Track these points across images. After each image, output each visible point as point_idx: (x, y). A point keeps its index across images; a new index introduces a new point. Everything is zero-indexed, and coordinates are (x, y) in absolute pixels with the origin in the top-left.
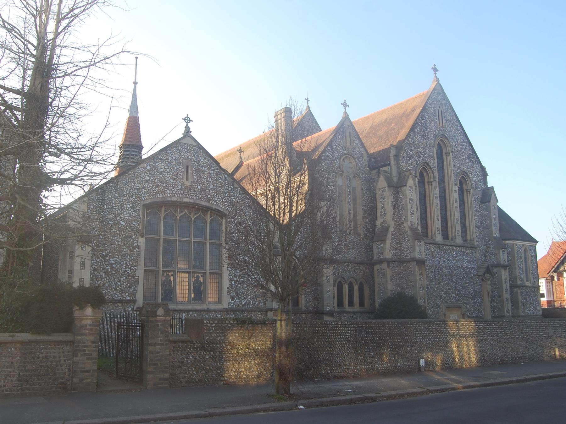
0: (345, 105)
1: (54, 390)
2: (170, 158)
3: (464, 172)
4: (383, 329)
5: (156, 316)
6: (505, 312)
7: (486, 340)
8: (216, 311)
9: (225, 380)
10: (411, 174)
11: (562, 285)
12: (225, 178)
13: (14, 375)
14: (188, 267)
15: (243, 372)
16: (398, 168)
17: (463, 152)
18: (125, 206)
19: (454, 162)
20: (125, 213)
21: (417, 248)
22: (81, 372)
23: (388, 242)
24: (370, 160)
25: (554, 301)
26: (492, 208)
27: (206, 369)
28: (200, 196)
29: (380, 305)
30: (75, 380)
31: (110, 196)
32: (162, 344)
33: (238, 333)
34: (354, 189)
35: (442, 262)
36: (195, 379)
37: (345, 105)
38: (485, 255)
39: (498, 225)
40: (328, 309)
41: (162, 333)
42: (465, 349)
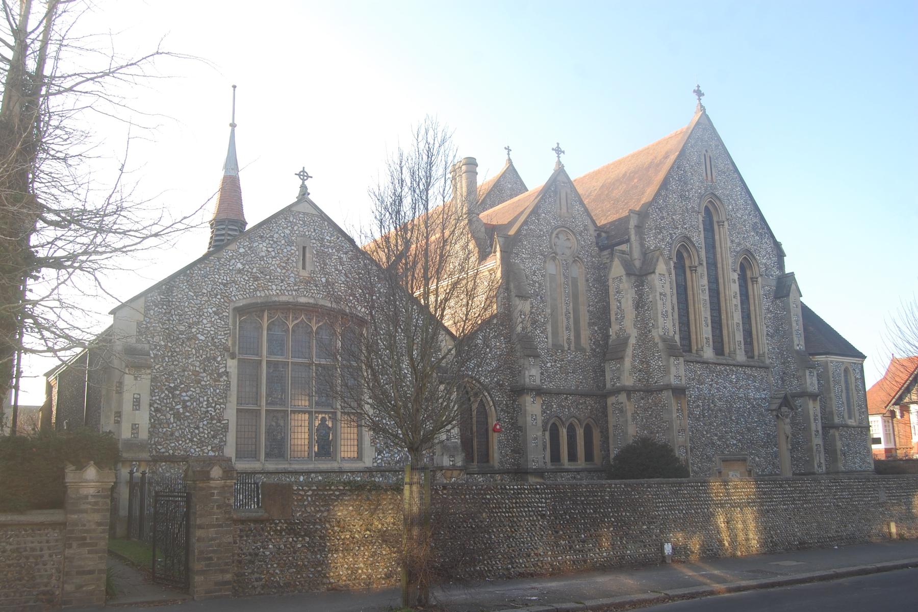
0: (558, 151)
1: (31, 603)
2: (276, 236)
3: (748, 251)
4: (601, 496)
5: (209, 479)
6: (816, 466)
8: (352, 472)
9: (331, 583)
10: (661, 254)
11: (908, 423)
14: (307, 404)
15: (362, 569)
16: (642, 245)
17: (745, 221)
19: (731, 235)
20: (205, 321)
21: (673, 370)
22: (79, 573)
23: (628, 362)
24: (599, 236)
25: (896, 449)
26: (792, 305)
27: (297, 565)
29: (617, 457)
30: (68, 588)
31: (180, 296)
32: (220, 526)
33: (352, 506)
34: (575, 281)
35: (714, 391)
36: (278, 582)
37: (558, 151)
38: (782, 378)
39: (802, 331)
40: (533, 466)
41: (219, 507)
42: (740, 526)
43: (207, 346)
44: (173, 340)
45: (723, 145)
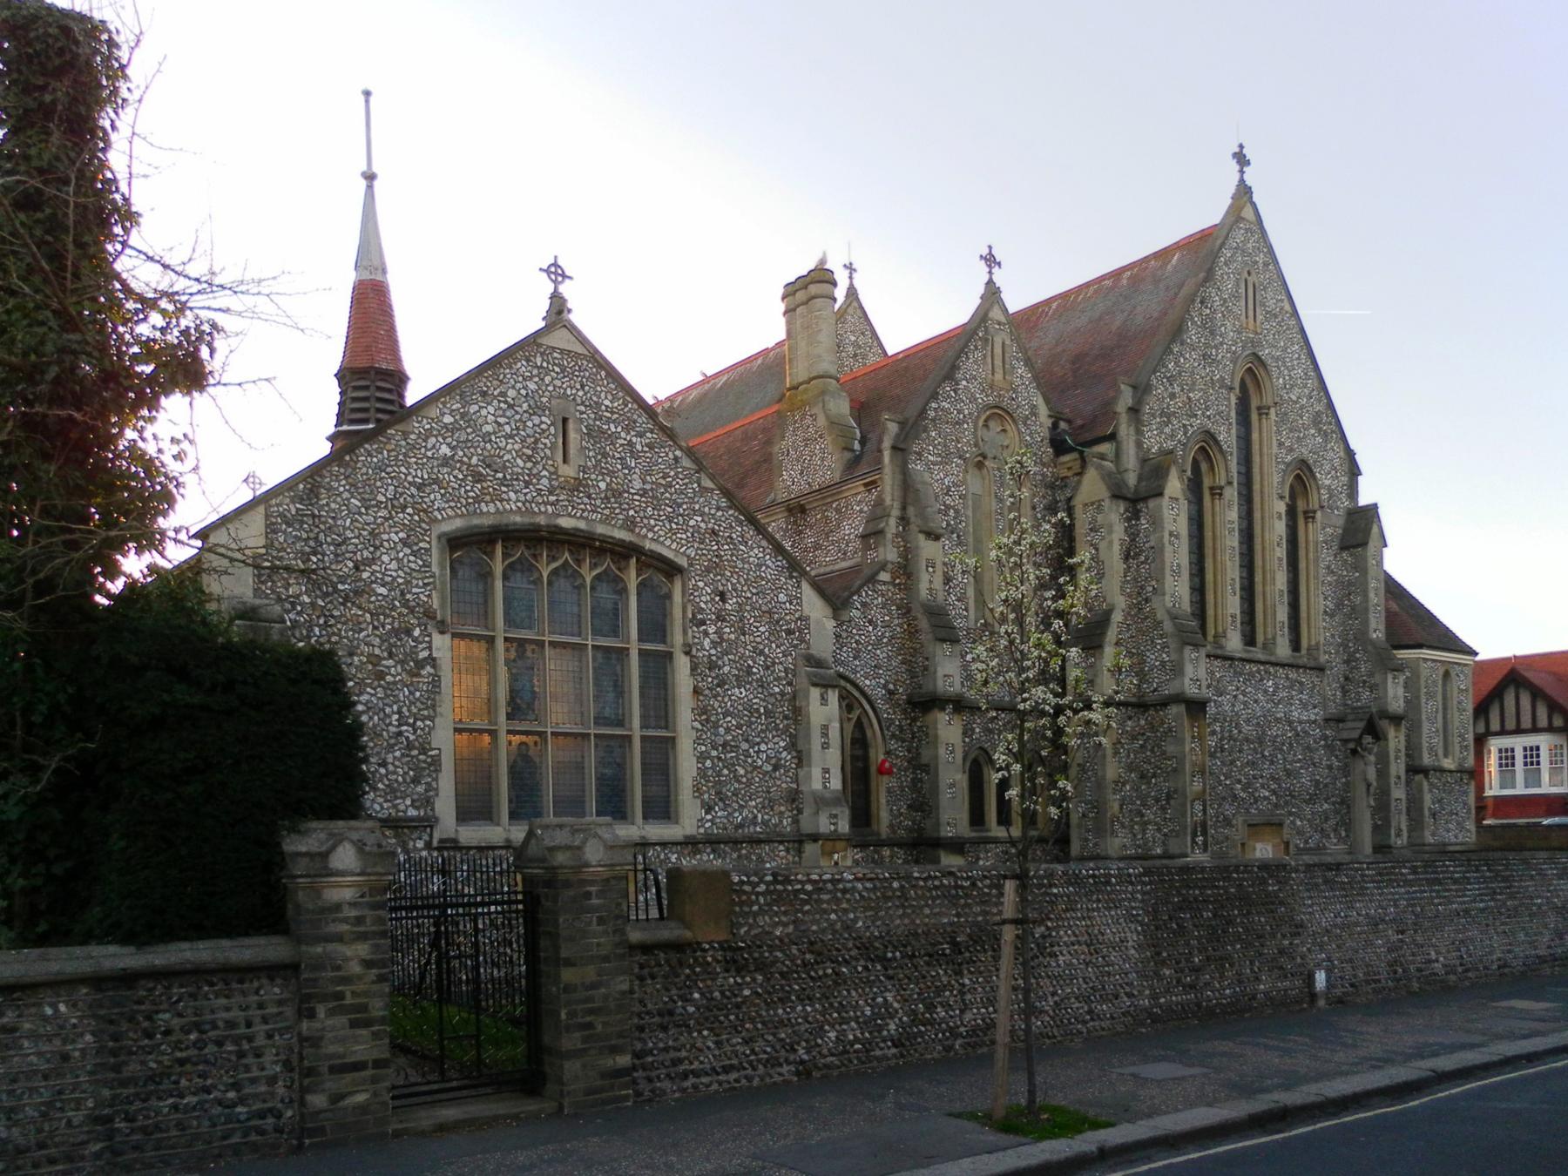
1: (235, 1139)
2: (511, 393)
3: (1303, 464)
4: (1223, 887)
7: (1467, 912)
8: (664, 845)
12: (676, 459)
13: (78, 1102)
16: (1139, 444)
17: (1302, 408)
18: (385, 537)
20: (385, 558)
21: (1189, 670)
22: (334, 1070)
28: (607, 512)
30: (317, 1101)
32: (606, 959)
37: (990, 260)
40: (948, 832)
43: (394, 608)
44: (327, 594)
45: (1276, 263)
